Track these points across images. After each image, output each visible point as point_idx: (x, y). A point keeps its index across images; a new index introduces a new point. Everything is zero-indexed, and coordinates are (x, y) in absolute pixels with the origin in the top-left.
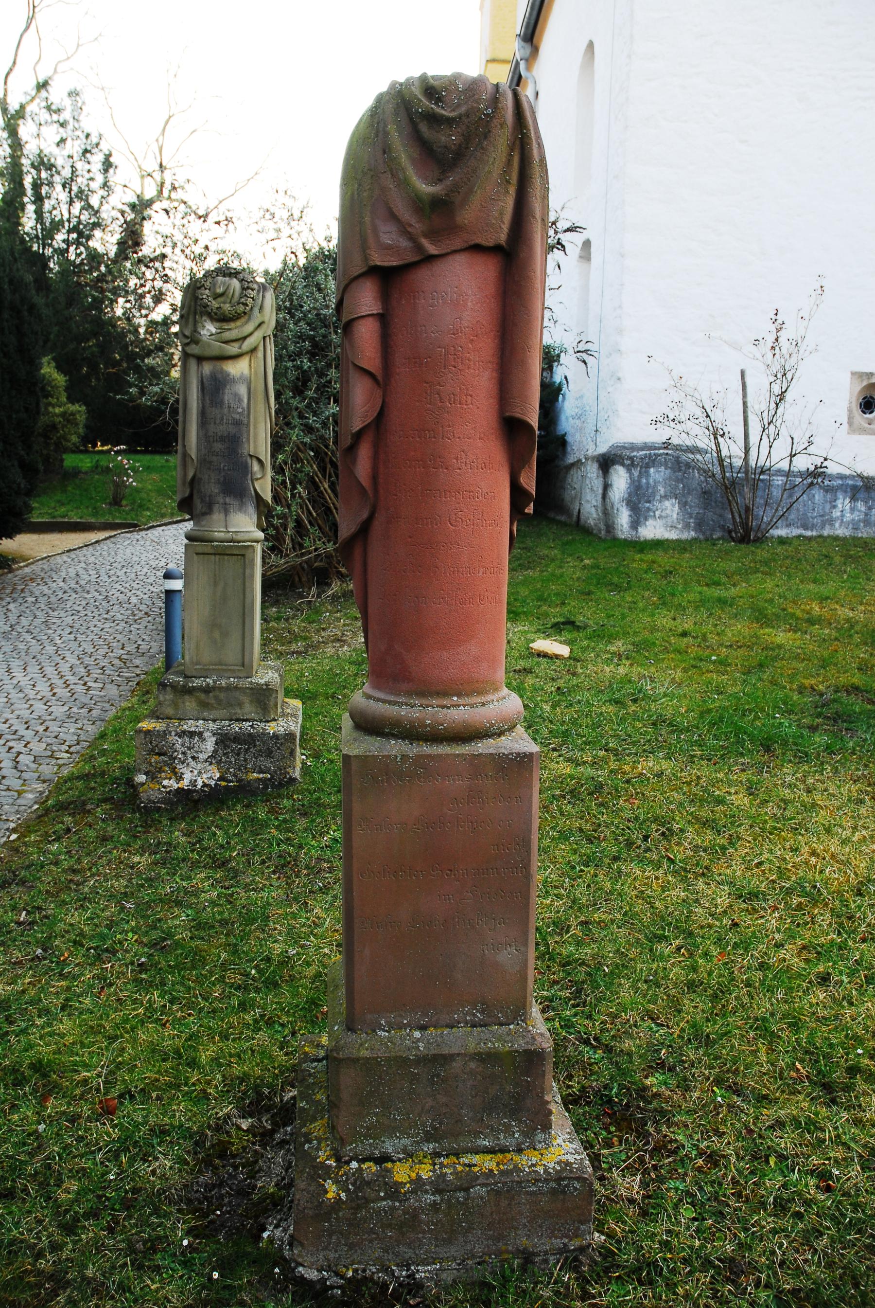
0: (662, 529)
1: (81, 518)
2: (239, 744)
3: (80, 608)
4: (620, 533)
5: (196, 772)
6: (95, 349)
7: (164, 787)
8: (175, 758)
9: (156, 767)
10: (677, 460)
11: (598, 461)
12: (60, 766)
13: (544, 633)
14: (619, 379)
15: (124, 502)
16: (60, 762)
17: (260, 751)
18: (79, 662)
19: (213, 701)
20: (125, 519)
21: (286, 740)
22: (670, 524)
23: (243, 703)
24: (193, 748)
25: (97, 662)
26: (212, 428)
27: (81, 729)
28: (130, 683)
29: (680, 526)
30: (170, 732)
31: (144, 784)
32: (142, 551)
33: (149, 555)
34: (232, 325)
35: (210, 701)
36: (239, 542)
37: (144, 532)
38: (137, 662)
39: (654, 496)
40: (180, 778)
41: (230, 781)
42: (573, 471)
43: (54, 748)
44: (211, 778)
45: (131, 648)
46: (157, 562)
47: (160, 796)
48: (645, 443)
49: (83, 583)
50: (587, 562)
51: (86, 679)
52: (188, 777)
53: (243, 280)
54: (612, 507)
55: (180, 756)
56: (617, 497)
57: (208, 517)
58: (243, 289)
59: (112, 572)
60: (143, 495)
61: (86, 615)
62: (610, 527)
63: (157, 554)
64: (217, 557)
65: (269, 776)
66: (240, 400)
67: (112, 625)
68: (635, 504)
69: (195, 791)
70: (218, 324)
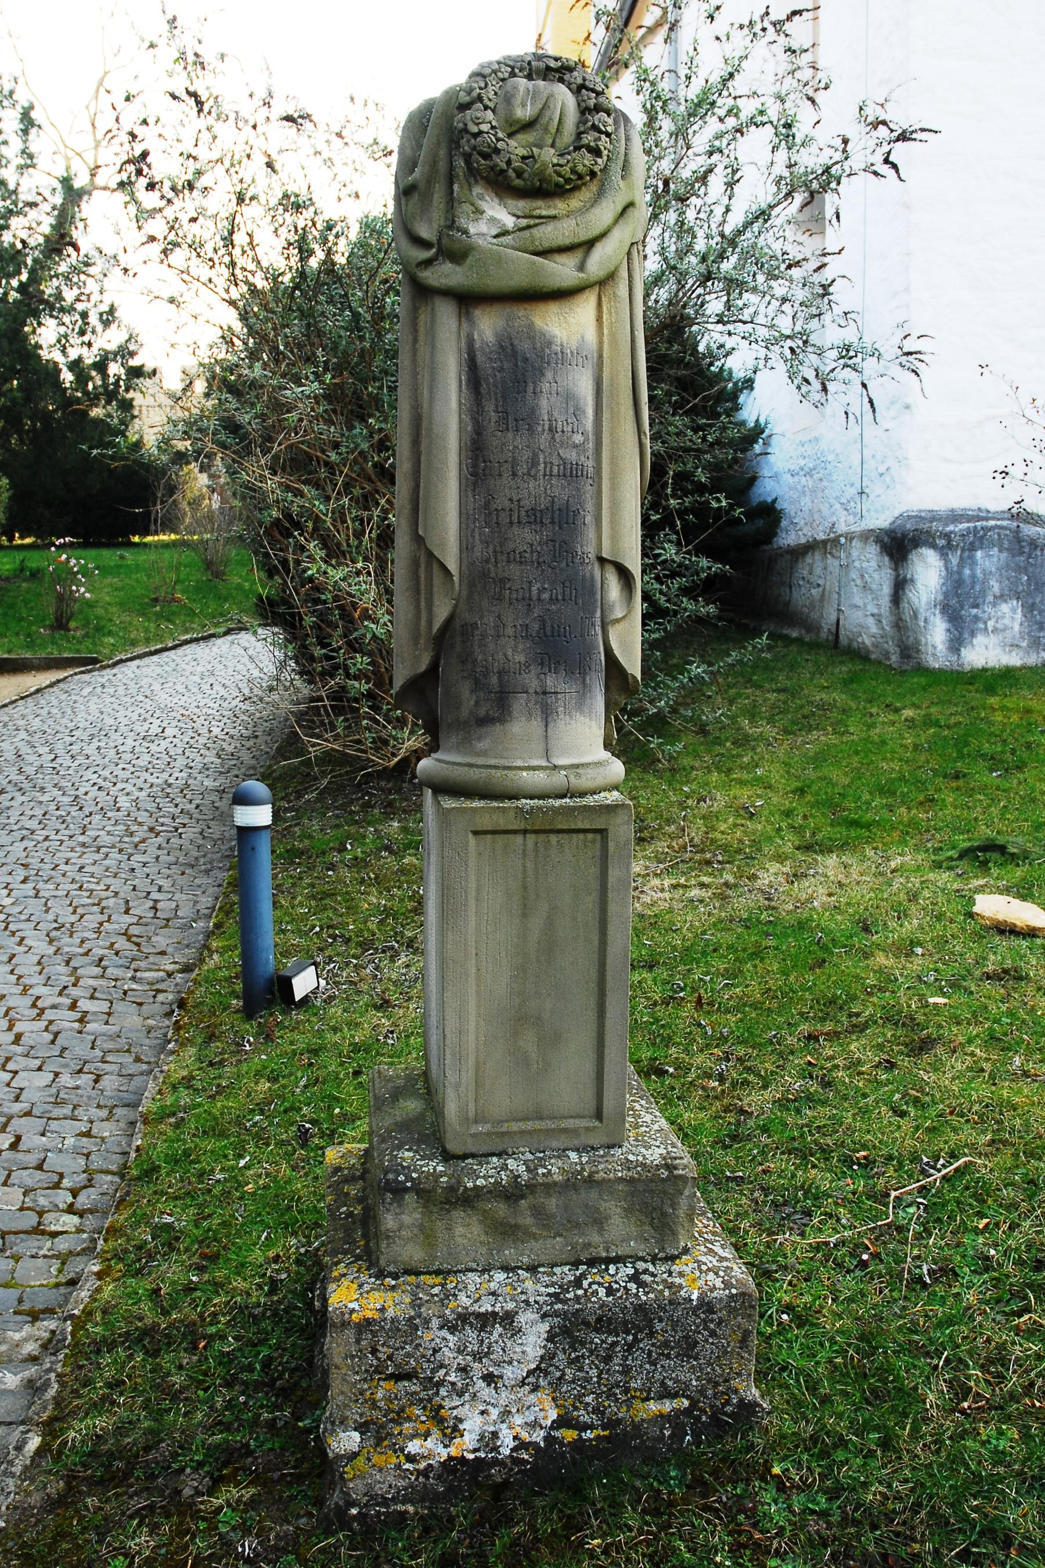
0: (998, 650)
1: (9, 652)
2: (610, 1333)
3: (33, 824)
4: (930, 659)
5: (494, 1413)
6: (18, 394)
7: (411, 1458)
8: (441, 1383)
9: (390, 1411)
10: (1017, 536)
11: (878, 540)
12: (64, 1258)
13: (950, 868)
14: (908, 407)
15: (72, 624)
16: (63, 1244)
17: (666, 1344)
18: (51, 950)
19: (527, 1220)
20: (78, 651)
21: (732, 1311)
22: (1009, 641)
23: (607, 1218)
24: (487, 1355)
25: (87, 946)
26: (505, 489)
27: (88, 1134)
28: (161, 997)
29: (1024, 644)
30: (427, 1321)
31: (354, 1455)
32: (115, 706)
33: (128, 713)
34: (559, 206)
35: (521, 1221)
36: (582, 794)
37: (108, 672)
38: (161, 941)
39: (984, 597)
40: (452, 1431)
41: (585, 1427)
42: (815, 561)
43: (42, 1201)
44: (534, 1425)
45: (141, 908)
46: (146, 726)
47: (402, 1483)
48: (952, 511)
49: (30, 770)
50: (908, 713)
51: (74, 992)
52: (473, 1426)
53: (582, 87)
54: (915, 616)
55: (452, 1378)
56: (924, 600)
57: (498, 728)
58: (584, 111)
59: (75, 749)
60: (100, 611)
61: (47, 838)
62: (909, 650)
63: (142, 711)
64: (531, 838)
65: (686, 1403)
66: (578, 412)
67: (97, 857)
68: (954, 611)
69: (495, 1462)
70: (522, 205)
